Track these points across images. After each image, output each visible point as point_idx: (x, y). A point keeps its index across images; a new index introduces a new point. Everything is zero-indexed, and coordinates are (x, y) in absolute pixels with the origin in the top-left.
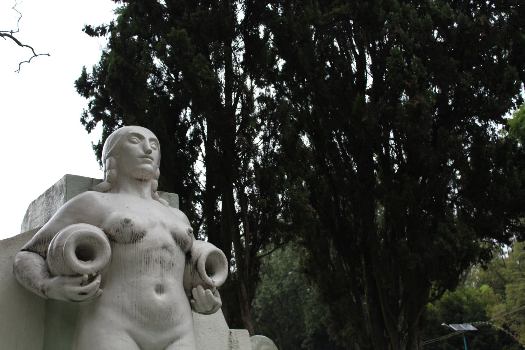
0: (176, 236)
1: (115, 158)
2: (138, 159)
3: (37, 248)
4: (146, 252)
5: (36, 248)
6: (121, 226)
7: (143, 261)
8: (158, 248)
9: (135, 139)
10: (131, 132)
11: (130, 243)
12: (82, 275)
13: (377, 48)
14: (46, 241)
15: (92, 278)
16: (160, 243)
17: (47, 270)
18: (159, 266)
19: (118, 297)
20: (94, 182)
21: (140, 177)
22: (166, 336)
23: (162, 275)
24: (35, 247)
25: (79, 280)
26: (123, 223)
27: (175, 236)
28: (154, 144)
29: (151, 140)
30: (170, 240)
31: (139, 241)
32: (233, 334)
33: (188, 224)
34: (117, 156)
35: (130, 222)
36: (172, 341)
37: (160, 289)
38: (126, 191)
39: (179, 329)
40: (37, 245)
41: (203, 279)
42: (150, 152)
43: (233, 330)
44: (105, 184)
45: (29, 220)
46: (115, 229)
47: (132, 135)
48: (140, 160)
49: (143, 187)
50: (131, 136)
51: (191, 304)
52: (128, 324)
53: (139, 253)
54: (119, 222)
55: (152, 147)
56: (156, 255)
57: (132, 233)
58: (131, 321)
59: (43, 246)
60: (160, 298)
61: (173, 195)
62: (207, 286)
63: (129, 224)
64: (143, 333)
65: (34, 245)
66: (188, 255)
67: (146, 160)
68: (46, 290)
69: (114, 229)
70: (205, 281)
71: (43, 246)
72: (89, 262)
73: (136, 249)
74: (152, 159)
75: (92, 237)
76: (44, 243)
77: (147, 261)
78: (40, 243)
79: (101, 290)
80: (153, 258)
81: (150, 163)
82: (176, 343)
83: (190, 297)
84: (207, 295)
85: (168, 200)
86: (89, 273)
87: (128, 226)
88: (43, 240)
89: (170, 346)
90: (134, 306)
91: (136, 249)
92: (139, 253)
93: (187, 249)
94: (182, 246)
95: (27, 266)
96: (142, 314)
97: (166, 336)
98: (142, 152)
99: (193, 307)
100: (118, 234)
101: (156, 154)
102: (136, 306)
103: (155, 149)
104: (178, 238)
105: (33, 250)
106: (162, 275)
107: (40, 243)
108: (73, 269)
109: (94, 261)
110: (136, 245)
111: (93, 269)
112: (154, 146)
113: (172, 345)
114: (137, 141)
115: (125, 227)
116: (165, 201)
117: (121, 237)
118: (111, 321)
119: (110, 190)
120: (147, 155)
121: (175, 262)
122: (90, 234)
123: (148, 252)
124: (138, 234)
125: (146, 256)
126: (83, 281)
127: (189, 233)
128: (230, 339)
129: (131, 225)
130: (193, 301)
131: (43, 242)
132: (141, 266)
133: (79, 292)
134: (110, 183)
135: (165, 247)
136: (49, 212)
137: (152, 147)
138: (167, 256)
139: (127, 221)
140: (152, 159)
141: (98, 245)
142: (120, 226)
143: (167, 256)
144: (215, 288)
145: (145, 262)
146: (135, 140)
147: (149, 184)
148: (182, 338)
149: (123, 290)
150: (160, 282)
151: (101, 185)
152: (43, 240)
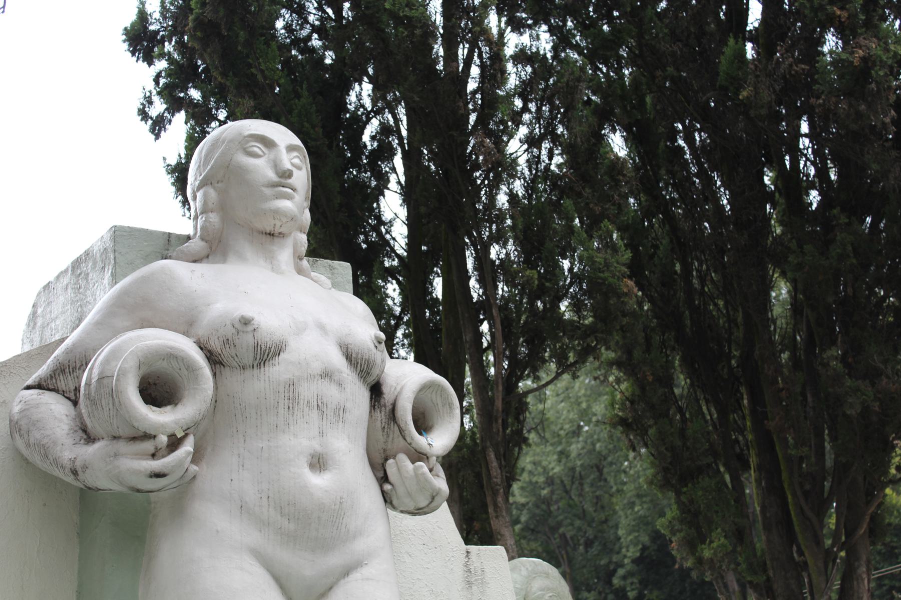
0: (349, 350)
1: (214, 188)
2: (264, 189)
3: (58, 382)
4: (287, 386)
5: (57, 383)
6: (234, 331)
7: (281, 405)
8: (311, 378)
9: (257, 148)
10: (247, 133)
14: (76, 368)
15: (174, 443)
16: (317, 367)
17: (81, 428)
18: (315, 413)
20: (173, 241)
21: (268, 229)
22: (335, 560)
23: (322, 434)
24: (54, 381)
25: (148, 446)
26: (237, 325)
28: (298, 157)
29: (291, 148)
30: (338, 361)
31: (271, 361)
32: (473, 556)
33: (373, 324)
34: (220, 185)
35: (252, 322)
36: (346, 572)
37: (318, 463)
38: (242, 258)
39: (360, 546)
40: (57, 376)
41: (409, 440)
42: (288, 174)
43: (473, 548)
44: (196, 245)
45: (39, 324)
46: (221, 339)
47: (250, 139)
48: (268, 191)
49: (275, 248)
50: (248, 142)
51: (383, 493)
52: (253, 537)
53: (271, 388)
54: (228, 323)
55: (293, 165)
56: (308, 391)
57: (257, 346)
58: (260, 531)
59: (69, 377)
60: (318, 481)
61: (340, 264)
62: (418, 456)
63: (250, 328)
64: (287, 557)
66: (376, 390)
67: (281, 191)
70: (413, 445)
72: (168, 408)
73: (267, 379)
74: (294, 190)
75: (173, 356)
76: (73, 371)
77: (291, 405)
79: (194, 468)
81: (289, 197)
82: (356, 576)
83: (383, 479)
84: (418, 476)
85: (330, 275)
86: (170, 431)
88: (69, 366)
89: (342, 582)
90: (265, 499)
91: (267, 379)
92: (271, 388)
93: (372, 379)
94: (361, 371)
95: (38, 421)
96: (282, 516)
97: (335, 560)
98: (271, 175)
99: (387, 499)
100: (228, 349)
101: (302, 178)
103: (299, 168)
104: (354, 355)
106: (322, 434)
108: (136, 425)
109: (179, 406)
111: (176, 422)
112: (297, 161)
114: (260, 153)
115: (241, 333)
116: (323, 278)
118: (218, 531)
119: (208, 257)
120: (283, 181)
121: (348, 405)
123: (291, 385)
124: (270, 348)
125: (287, 395)
126: (156, 448)
127: (377, 344)
128: (466, 565)
129: (255, 329)
130: (387, 487)
131: (71, 370)
132: (277, 415)
133: (149, 472)
135: (327, 375)
136: (81, 306)
137: (293, 165)
138: (331, 392)
139: (246, 322)
140: (294, 190)
141: (186, 372)
143: (331, 392)
144: (435, 458)
146: (256, 149)
147: (289, 242)
148: (366, 564)
149: (241, 467)
150: (318, 448)
151: (187, 246)
152: (69, 366)
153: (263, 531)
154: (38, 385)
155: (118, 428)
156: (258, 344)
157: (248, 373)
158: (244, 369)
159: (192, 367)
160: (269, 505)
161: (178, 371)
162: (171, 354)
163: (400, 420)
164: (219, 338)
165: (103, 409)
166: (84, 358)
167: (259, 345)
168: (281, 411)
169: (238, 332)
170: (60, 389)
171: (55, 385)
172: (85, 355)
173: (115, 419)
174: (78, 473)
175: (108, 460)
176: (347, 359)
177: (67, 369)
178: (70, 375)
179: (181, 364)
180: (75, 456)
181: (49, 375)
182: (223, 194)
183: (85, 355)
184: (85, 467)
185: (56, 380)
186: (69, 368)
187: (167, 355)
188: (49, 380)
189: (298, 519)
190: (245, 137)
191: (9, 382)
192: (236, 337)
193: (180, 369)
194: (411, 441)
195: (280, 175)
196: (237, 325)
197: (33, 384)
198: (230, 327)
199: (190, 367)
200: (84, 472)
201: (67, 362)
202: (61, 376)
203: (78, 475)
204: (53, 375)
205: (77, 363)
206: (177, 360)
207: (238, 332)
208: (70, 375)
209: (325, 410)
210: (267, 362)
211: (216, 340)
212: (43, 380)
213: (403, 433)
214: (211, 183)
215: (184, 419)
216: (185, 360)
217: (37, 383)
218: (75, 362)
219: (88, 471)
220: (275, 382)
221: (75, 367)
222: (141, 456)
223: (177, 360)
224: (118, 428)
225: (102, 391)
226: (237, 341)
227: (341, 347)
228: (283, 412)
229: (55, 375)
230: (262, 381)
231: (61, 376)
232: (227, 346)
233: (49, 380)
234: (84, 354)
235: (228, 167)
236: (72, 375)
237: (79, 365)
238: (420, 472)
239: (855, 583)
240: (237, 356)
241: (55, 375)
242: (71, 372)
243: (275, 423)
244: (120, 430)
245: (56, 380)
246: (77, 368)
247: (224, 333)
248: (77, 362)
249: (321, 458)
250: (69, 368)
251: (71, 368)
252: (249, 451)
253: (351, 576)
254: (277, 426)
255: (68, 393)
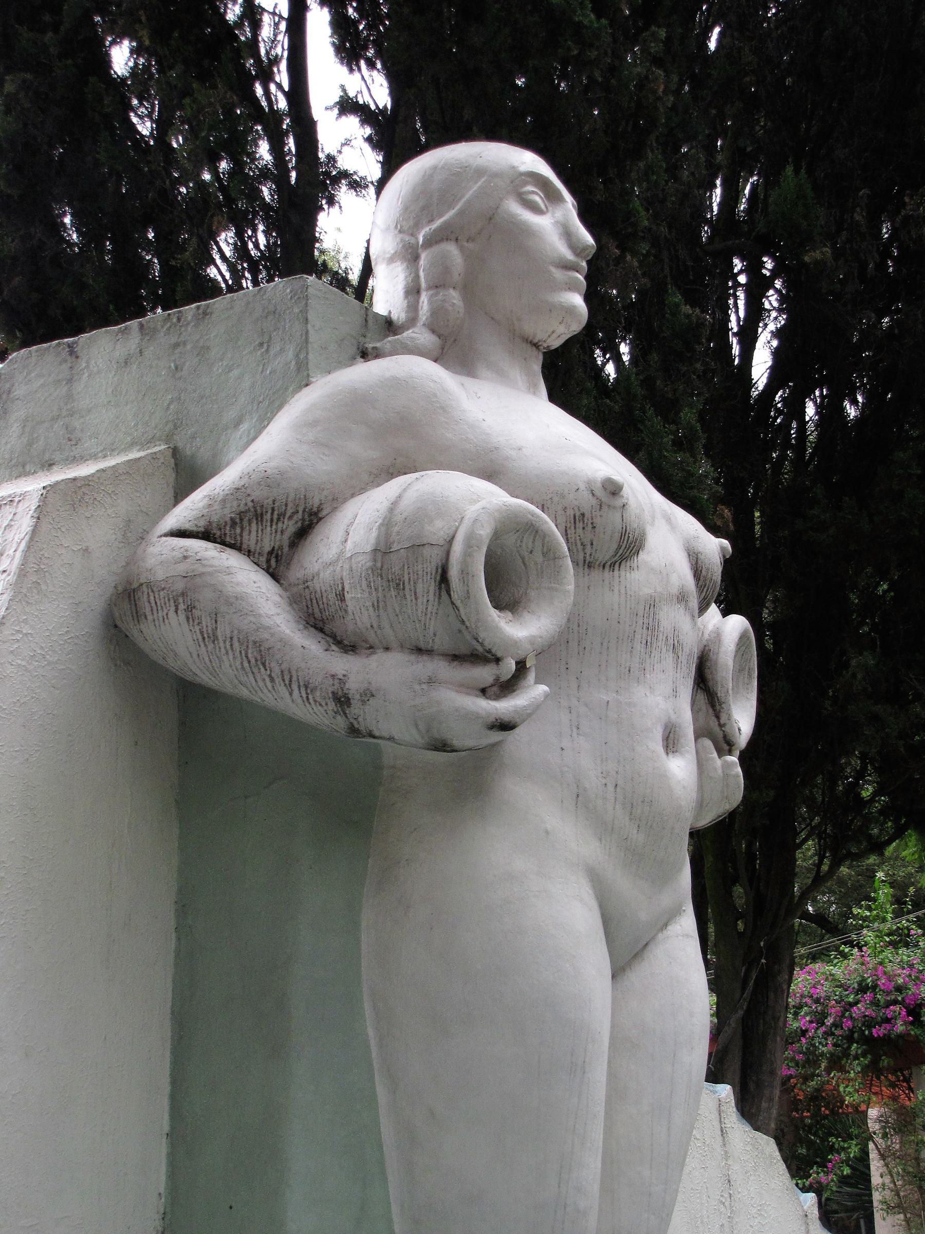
0: (699, 562)
1: (462, 249)
2: (553, 270)
3: (245, 534)
4: (647, 608)
5: (241, 536)
6: (594, 502)
7: (638, 636)
11: (604, 567)
12: (498, 660)
13: (775, 6)
14: (284, 516)
19: (562, 749)
24: (238, 530)
25: (485, 674)
26: (599, 493)
27: (697, 563)
31: (628, 564)
34: (470, 245)
38: (501, 376)
40: (245, 523)
46: (570, 512)
47: (529, 179)
48: (558, 274)
50: (525, 183)
53: (628, 606)
54: (582, 487)
58: (600, 840)
59: (269, 529)
65: (233, 523)
68: (358, 697)
69: (565, 509)
70: (727, 729)
71: (269, 529)
73: (623, 591)
75: (531, 529)
76: (278, 519)
77: (649, 640)
78: (259, 516)
80: (661, 629)
86: (521, 654)
87: (614, 508)
88: (273, 509)
90: (611, 788)
91: (623, 591)
92: (628, 606)
94: (704, 599)
95: (237, 598)
96: (631, 819)
100: (579, 531)
102: (618, 789)
104: (704, 572)
105: (228, 539)
107: (259, 516)
108: (482, 635)
109: (527, 616)
110: (622, 579)
111: (531, 640)
113: (665, 932)
115: (605, 508)
117: (587, 542)
118: (547, 832)
122: (530, 516)
123: (652, 604)
125: (646, 621)
129: (624, 505)
131: (275, 517)
132: (631, 652)
133: (492, 719)
134: (439, 336)
141: (540, 559)
142: (586, 502)
145: (644, 642)
149: (575, 730)
152: (273, 509)
153: (604, 842)
154: (203, 533)
155: (435, 635)
156: (626, 531)
157: (596, 574)
158: (589, 567)
159: (555, 553)
160: (616, 798)
161: (526, 554)
162: (532, 524)
163: (720, 686)
164: (565, 509)
165: (416, 599)
166: (302, 501)
167: (627, 532)
168: (639, 647)
169: (601, 506)
170: (245, 546)
171: (239, 539)
172: (305, 496)
173: (433, 618)
174: (352, 701)
175: (417, 687)
176: (695, 576)
177: (269, 515)
178: (271, 526)
179: (538, 543)
180: (345, 673)
181: (228, 519)
182: (475, 262)
183: (305, 496)
184: (368, 695)
185: (242, 529)
186: (272, 514)
187: (527, 524)
188: (228, 528)
189: (651, 827)
190: (522, 174)
191: (92, 516)
192: (598, 513)
193: (531, 552)
194: (727, 721)
195: (578, 251)
196: (599, 493)
197: (195, 529)
198: (586, 495)
199: (550, 553)
200: (364, 702)
201: (270, 501)
202: (254, 525)
203: (349, 705)
204: (238, 521)
205: (289, 508)
206: (535, 537)
207: (601, 506)
208: (271, 526)
209: (680, 654)
210: (623, 563)
211: (560, 512)
212: (214, 525)
213: (718, 707)
214: (457, 239)
215: (541, 637)
216: (547, 539)
217: (202, 529)
218: (286, 505)
219: (372, 701)
220: (633, 598)
221: (284, 514)
222: (466, 688)
223: (535, 537)
224: (435, 635)
225: (420, 566)
226: (598, 521)
227: (689, 555)
228: (639, 648)
229: (241, 520)
230: (616, 591)
231: (254, 525)
232: (580, 525)
233: (228, 528)
234: (303, 494)
235: (490, 219)
236: (274, 527)
237: (291, 511)
238: (733, 773)
239: (772, 995)
240: (592, 544)
241: (241, 520)
242: (275, 520)
243: (628, 665)
244: (437, 640)
245: (242, 529)
246: (287, 516)
247: (577, 503)
248: (290, 505)
249: (672, 731)
250: (272, 514)
251: (276, 513)
252: (586, 705)
253: (669, 928)
254: (629, 671)
255: (256, 555)
